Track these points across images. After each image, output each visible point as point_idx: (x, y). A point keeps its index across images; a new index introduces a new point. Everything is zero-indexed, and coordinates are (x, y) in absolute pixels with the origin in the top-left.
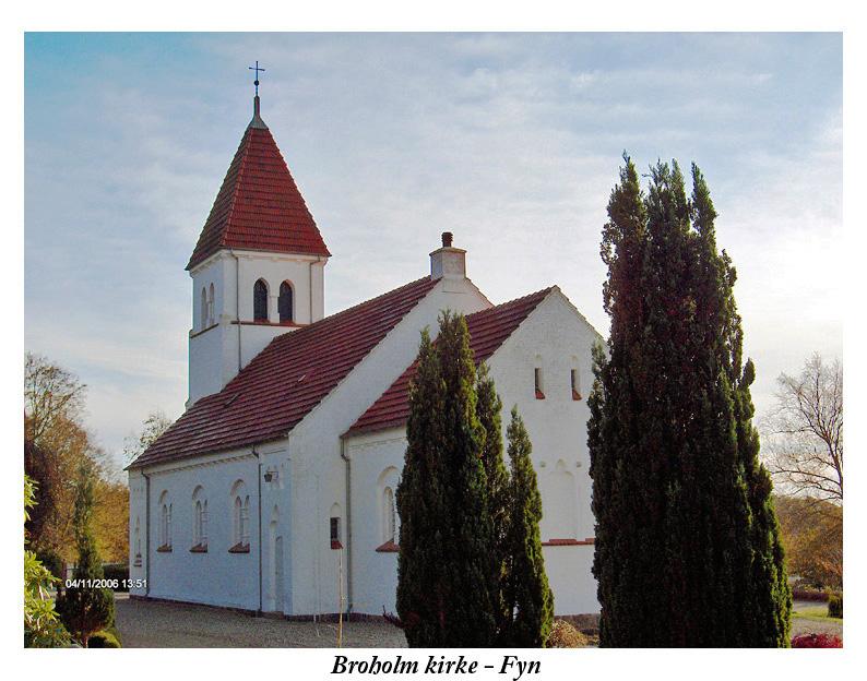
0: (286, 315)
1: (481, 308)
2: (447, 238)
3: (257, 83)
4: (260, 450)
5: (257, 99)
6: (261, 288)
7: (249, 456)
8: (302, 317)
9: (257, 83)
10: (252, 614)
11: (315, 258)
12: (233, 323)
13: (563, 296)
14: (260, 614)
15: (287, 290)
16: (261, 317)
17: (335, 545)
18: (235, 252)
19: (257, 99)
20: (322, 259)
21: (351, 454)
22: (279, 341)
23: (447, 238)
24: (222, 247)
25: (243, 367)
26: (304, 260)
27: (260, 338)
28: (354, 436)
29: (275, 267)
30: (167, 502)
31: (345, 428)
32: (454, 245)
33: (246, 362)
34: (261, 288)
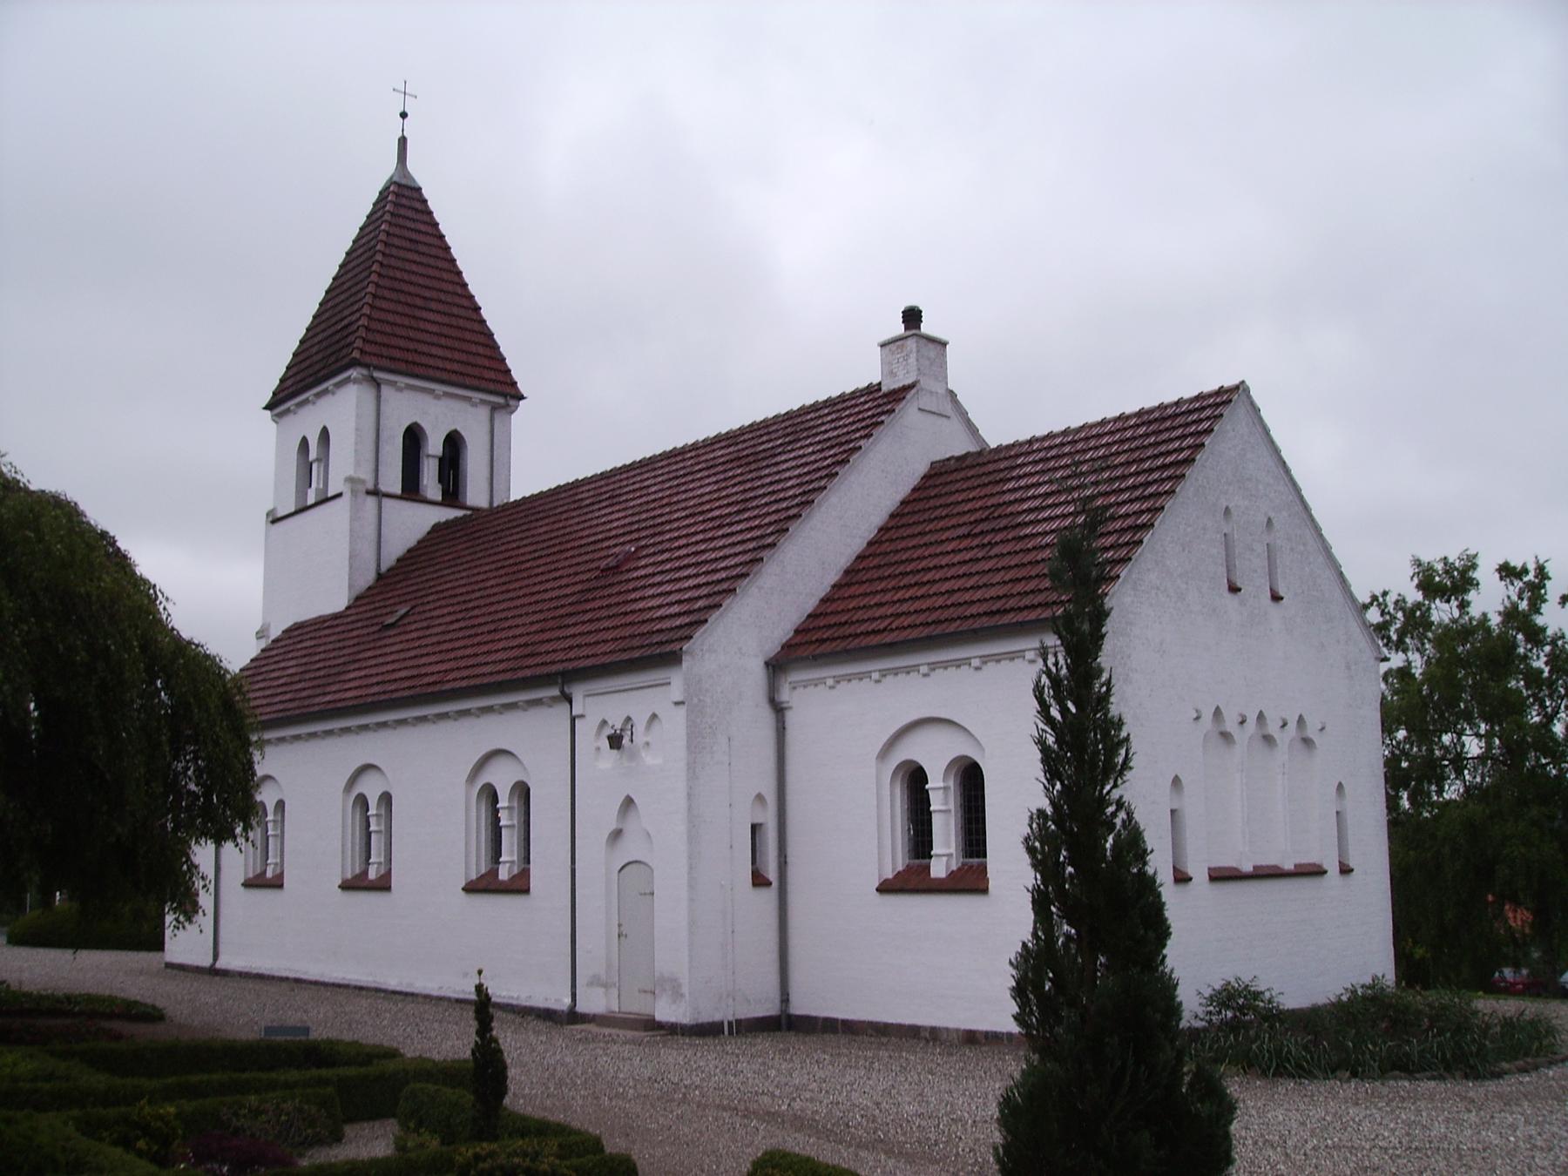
0: (452, 493)
1: (960, 446)
2: (912, 317)
3: (404, 115)
4: (578, 692)
5: (403, 142)
6: (414, 437)
7: (554, 699)
8: (476, 494)
9: (404, 115)
10: (547, 1015)
11: (501, 400)
12: (368, 493)
13: (1252, 404)
14: (574, 1016)
15: (454, 443)
16: (411, 490)
17: (759, 880)
18: (377, 374)
19: (403, 142)
20: (512, 402)
21: (785, 695)
22: (437, 528)
23: (912, 317)
24: (354, 363)
25: (384, 569)
26: (483, 402)
27: (412, 523)
28: (817, 660)
29: (440, 413)
30: (631, 849)
31: (772, 647)
32: (926, 328)
33: (389, 561)
34: (414, 437)
